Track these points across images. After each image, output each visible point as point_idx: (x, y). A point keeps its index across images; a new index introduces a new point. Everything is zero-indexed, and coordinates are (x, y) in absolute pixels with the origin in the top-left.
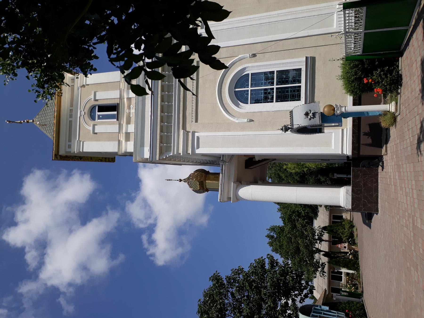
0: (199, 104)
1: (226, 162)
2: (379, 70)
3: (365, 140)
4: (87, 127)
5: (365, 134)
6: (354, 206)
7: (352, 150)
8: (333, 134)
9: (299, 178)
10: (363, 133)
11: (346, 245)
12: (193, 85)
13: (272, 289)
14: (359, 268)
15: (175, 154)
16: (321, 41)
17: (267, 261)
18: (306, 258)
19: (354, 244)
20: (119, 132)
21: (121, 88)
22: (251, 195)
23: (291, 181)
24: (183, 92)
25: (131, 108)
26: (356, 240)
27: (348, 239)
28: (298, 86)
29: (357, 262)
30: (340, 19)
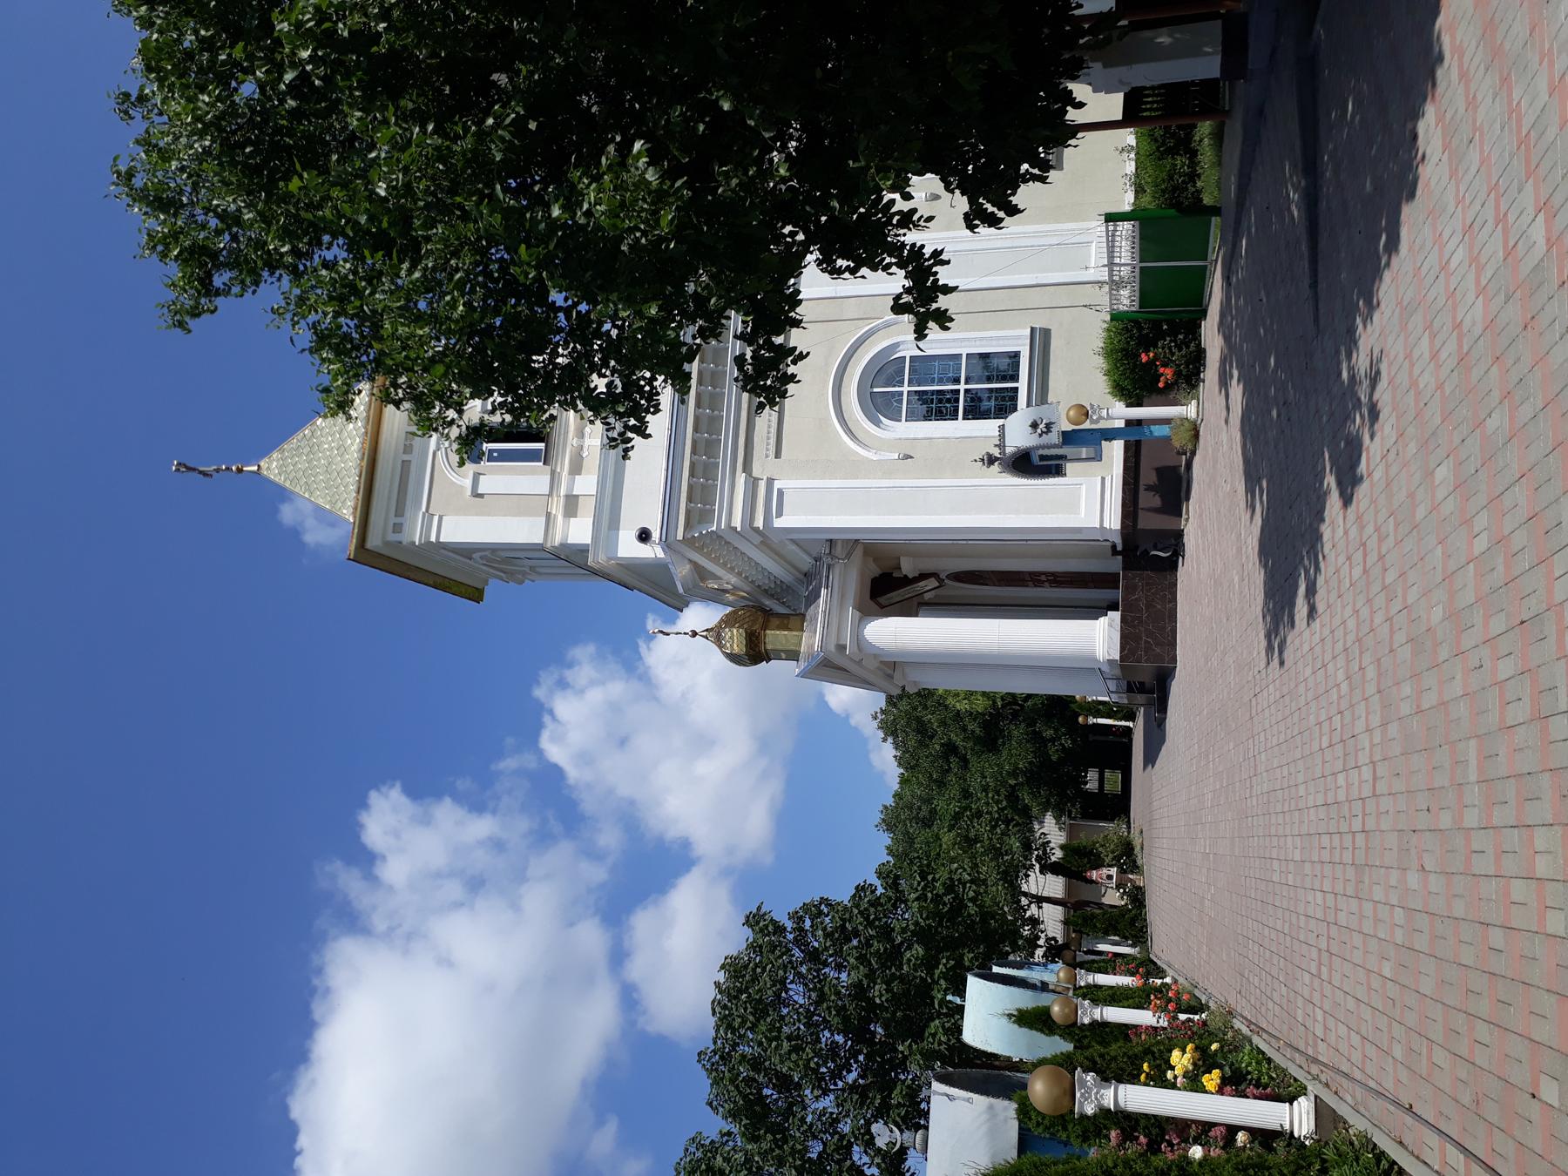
2: (1168, 339)
3: (1148, 499)
4: (453, 477)
5: (1149, 488)
8: (1084, 487)
11: (1113, 871)
16: (1063, 297)
19: (1135, 868)
20: (550, 495)
23: (957, 736)
25: (587, 435)
27: (1117, 859)
28: (1011, 388)
30: (1101, 250)
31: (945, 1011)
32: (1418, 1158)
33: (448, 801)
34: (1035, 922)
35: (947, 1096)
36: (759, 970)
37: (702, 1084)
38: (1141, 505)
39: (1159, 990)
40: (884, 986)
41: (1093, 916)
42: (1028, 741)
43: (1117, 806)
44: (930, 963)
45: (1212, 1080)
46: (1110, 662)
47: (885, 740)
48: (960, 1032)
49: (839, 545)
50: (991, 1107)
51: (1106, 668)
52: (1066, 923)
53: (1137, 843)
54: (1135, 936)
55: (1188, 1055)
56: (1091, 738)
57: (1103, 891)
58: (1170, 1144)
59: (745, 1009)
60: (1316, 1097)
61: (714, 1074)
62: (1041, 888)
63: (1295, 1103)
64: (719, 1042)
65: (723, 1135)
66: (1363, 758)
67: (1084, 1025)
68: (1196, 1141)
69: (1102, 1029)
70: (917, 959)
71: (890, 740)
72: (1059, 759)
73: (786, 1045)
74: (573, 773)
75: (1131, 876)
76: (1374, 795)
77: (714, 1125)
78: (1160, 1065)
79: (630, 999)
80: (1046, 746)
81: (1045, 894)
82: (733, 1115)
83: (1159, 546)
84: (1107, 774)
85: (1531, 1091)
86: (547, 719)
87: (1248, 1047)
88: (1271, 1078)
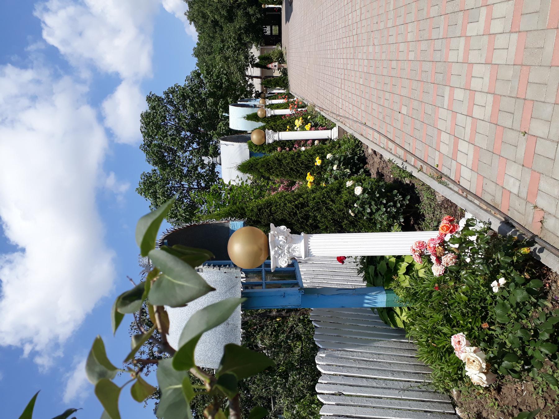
5: (388, 287)
11: (276, 64)
27: (278, 59)
31: (223, 118)
32: (366, 138)
33: (9, 65)
34: (251, 85)
35: (226, 144)
36: (155, 114)
37: (143, 156)
39: (292, 103)
40: (201, 113)
41: (271, 81)
42: (244, 16)
43: (277, 39)
44: (215, 104)
45: (308, 127)
47: (191, 24)
48: (229, 125)
50: (240, 146)
52: (262, 84)
53: (284, 52)
54: (285, 86)
55: (300, 121)
56: (267, 13)
57: (274, 71)
58: (295, 148)
59: (153, 128)
60: (339, 126)
61: (146, 151)
62: (252, 73)
63: (333, 129)
64: (146, 141)
65: (153, 171)
66: (358, 7)
67: (268, 117)
68: (303, 146)
69: (274, 117)
70: (211, 103)
71: (192, 23)
72: (255, 22)
73: (169, 138)
74: (62, 49)
75: (282, 65)
76: (361, 20)
77: (149, 168)
78: (293, 126)
79: (109, 133)
80: (250, 18)
81: (254, 75)
82: (155, 164)
84: (273, 27)
85: (399, 111)
86: (43, 25)
87: (319, 115)
88: (326, 124)
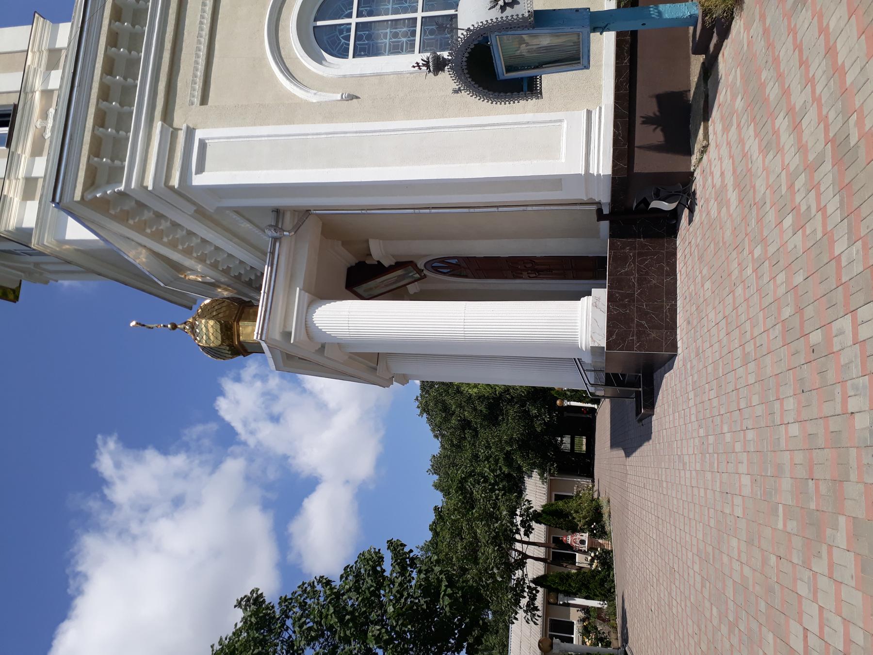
0: (216, 61)
1: (284, 231)
5: (647, 121)
6: (614, 337)
7: (613, 161)
8: (565, 124)
9: (486, 408)
10: (641, 117)
11: (585, 536)
12: (203, 11)
13: (400, 622)
14: (614, 591)
15: (133, 186)
17: (388, 556)
18: (492, 569)
21: (29, 66)
22: (347, 322)
24: (173, 26)
26: (608, 524)
27: (589, 523)
29: (609, 577)
38: (637, 143)
46: (595, 350)
49: (288, 216)
51: (587, 359)
56: (566, 414)
80: (532, 421)
83: (663, 194)
